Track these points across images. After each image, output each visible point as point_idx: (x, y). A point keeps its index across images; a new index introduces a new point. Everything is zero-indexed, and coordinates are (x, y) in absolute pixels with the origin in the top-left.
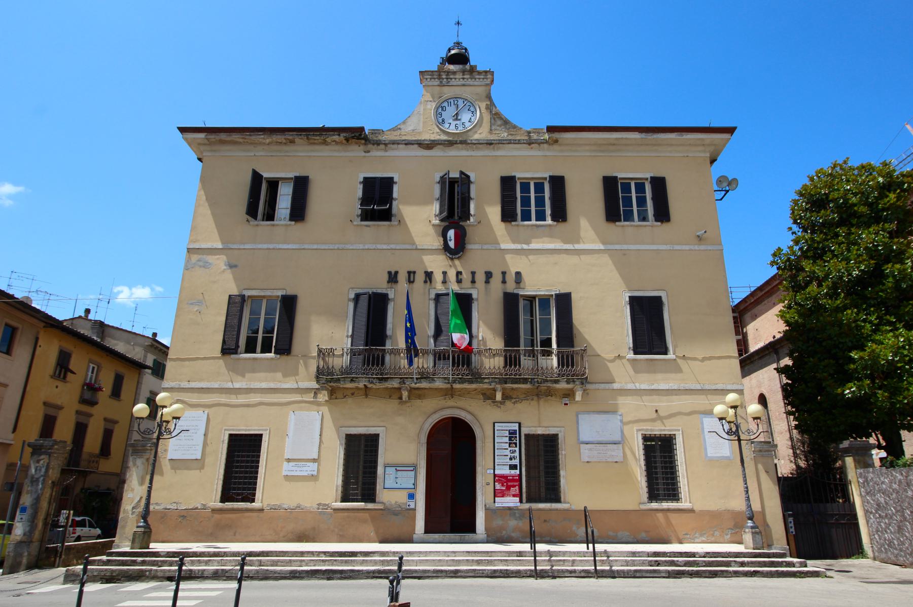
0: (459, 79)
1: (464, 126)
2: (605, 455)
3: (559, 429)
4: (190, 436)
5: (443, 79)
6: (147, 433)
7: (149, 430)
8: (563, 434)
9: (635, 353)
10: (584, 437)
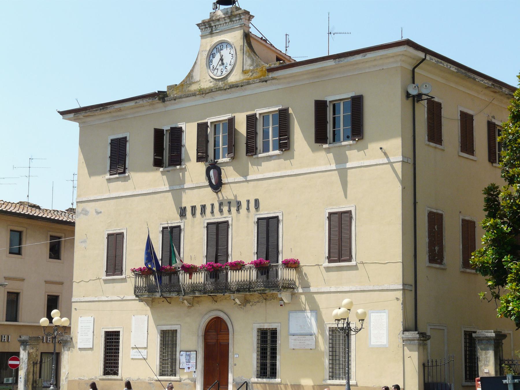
0: (223, 24)
1: (226, 70)
2: (304, 344)
3: (277, 324)
4: (87, 333)
5: (213, 26)
6: (49, 335)
7: (50, 333)
8: (279, 328)
9: (330, 262)
10: (292, 331)
